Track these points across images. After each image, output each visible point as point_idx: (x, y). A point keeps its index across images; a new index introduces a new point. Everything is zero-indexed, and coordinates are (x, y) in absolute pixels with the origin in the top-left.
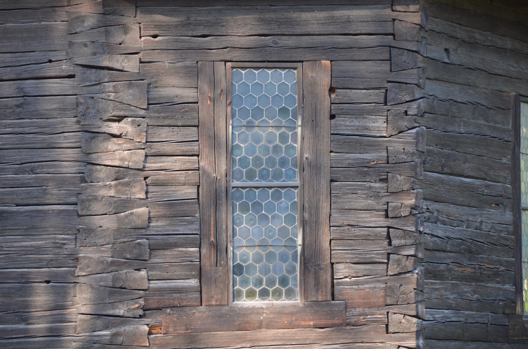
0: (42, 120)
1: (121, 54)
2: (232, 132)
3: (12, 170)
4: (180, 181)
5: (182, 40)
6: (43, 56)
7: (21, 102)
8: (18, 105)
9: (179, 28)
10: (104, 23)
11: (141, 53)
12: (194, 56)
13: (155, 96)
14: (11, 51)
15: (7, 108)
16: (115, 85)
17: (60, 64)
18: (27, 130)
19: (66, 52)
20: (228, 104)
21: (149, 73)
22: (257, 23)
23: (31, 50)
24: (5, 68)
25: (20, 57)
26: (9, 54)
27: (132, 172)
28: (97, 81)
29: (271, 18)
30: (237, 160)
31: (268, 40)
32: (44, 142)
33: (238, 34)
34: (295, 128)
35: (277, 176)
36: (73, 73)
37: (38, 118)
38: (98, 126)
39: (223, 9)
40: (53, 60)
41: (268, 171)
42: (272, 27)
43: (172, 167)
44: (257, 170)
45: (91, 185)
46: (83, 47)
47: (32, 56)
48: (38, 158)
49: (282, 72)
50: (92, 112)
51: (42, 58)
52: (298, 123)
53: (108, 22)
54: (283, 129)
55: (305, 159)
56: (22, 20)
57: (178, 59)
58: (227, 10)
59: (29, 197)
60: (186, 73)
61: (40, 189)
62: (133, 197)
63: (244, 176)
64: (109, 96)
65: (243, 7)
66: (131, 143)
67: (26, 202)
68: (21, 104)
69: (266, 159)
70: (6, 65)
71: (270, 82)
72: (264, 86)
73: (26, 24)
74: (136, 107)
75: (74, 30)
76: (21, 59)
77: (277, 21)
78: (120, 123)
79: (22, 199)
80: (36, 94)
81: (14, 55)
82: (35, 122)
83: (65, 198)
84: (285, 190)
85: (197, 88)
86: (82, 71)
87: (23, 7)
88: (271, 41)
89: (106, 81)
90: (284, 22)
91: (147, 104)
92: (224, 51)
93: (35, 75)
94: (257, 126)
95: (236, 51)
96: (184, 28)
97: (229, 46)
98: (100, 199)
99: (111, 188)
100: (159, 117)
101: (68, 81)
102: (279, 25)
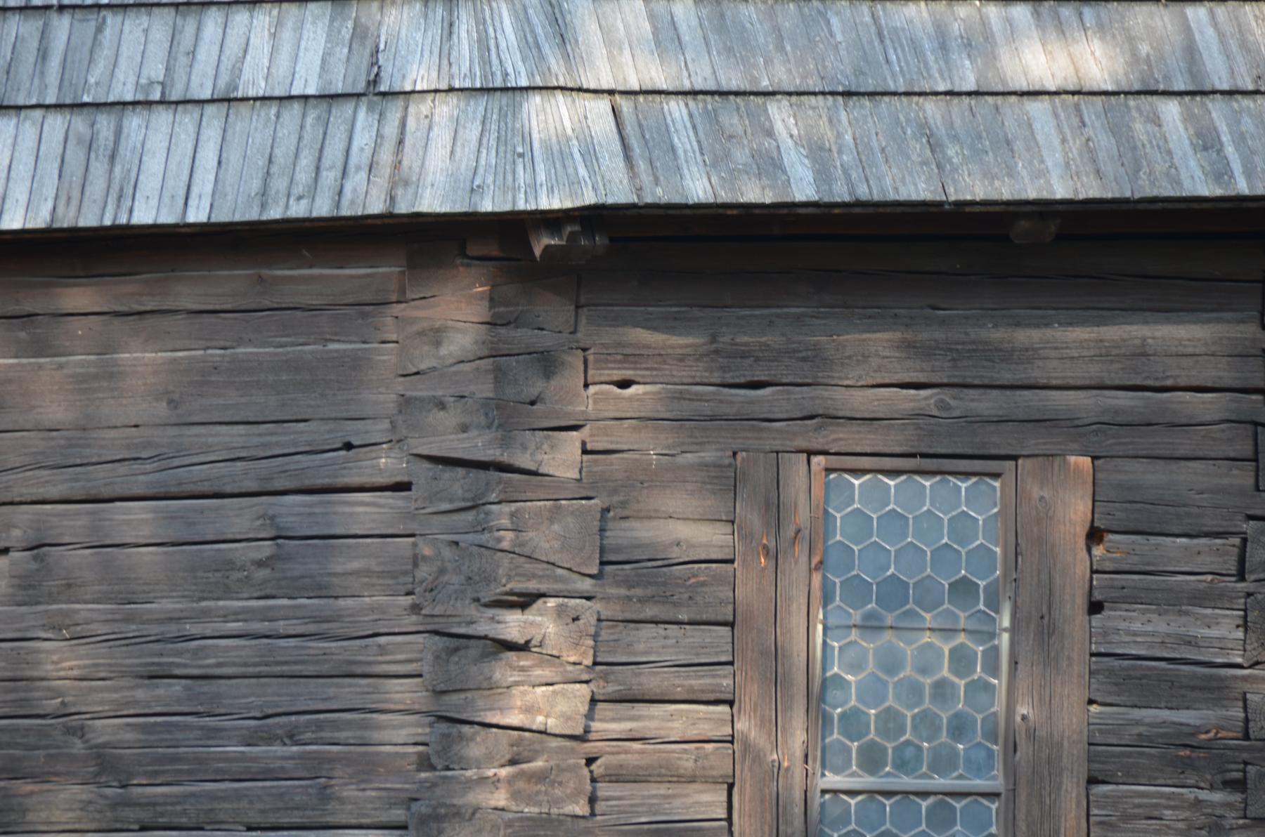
0: (322, 601)
2: (825, 643)
3: (237, 733)
4: (682, 771)
5: (696, 394)
6: (330, 432)
8: (261, 560)
9: (691, 363)
10: (492, 349)
13: (620, 541)
15: (232, 569)
16: (517, 510)
17: (374, 455)
18: (281, 626)
19: (391, 422)
20: (813, 566)
21: (607, 481)
24: (229, 464)
25: (271, 434)
26: (241, 427)
27: (554, 743)
28: (468, 500)
29: (935, 340)
30: (836, 716)
31: (926, 398)
32: (326, 660)
34: (992, 635)
35: (943, 763)
36: (405, 479)
37: (312, 595)
38: (469, 619)
40: (355, 443)
41: (919, 748)
42: (937, 363)
43: (662, 733)
44: (890, 746)
45: (445, 777)
46: (435, 410)
47: (302, 432)
48: (310, 702)
49: (959, 483)
50: (452, 582)
51: (327, 436)
52: (1001, 620)
53: (501, 346)
54: (962, 638)
55: (1018, 719)
56: (278, 339)
57: (683, 444)
58: (817, 318)
59: (280, 805)
60: (704, 483)
61: (311, 786)
62: (555, 811)
63: (854, 762)
64: (499, 540)
65: (861, 311)
66: (553, 665)
67: (273, 820)
68: (268, 558)
69: (914, 718)
71: (929, 510)
72: (911, 521)
74: (570, 569)
75: (413, 365)
76: (274, 439)
77: (950, 350)
78: (527, 612)
79: (262, 811)
80: (309, 533)
81: (255, 429)
82: (304, 606)
83: (375, 809)
84: (965, 802)
85: (733, 522)
87: (284, 306)
88: (932, 401)
90: (969, 351)
91: (598, 561)
92: (806, 425)
93: (307, 483)
94: (891, 627)
95: (838, 425)
96: (700, 364)
97: (821, 412)
98: (467, 816)
99: (499, 785)
100: (629, 598)
102: (954, 360)
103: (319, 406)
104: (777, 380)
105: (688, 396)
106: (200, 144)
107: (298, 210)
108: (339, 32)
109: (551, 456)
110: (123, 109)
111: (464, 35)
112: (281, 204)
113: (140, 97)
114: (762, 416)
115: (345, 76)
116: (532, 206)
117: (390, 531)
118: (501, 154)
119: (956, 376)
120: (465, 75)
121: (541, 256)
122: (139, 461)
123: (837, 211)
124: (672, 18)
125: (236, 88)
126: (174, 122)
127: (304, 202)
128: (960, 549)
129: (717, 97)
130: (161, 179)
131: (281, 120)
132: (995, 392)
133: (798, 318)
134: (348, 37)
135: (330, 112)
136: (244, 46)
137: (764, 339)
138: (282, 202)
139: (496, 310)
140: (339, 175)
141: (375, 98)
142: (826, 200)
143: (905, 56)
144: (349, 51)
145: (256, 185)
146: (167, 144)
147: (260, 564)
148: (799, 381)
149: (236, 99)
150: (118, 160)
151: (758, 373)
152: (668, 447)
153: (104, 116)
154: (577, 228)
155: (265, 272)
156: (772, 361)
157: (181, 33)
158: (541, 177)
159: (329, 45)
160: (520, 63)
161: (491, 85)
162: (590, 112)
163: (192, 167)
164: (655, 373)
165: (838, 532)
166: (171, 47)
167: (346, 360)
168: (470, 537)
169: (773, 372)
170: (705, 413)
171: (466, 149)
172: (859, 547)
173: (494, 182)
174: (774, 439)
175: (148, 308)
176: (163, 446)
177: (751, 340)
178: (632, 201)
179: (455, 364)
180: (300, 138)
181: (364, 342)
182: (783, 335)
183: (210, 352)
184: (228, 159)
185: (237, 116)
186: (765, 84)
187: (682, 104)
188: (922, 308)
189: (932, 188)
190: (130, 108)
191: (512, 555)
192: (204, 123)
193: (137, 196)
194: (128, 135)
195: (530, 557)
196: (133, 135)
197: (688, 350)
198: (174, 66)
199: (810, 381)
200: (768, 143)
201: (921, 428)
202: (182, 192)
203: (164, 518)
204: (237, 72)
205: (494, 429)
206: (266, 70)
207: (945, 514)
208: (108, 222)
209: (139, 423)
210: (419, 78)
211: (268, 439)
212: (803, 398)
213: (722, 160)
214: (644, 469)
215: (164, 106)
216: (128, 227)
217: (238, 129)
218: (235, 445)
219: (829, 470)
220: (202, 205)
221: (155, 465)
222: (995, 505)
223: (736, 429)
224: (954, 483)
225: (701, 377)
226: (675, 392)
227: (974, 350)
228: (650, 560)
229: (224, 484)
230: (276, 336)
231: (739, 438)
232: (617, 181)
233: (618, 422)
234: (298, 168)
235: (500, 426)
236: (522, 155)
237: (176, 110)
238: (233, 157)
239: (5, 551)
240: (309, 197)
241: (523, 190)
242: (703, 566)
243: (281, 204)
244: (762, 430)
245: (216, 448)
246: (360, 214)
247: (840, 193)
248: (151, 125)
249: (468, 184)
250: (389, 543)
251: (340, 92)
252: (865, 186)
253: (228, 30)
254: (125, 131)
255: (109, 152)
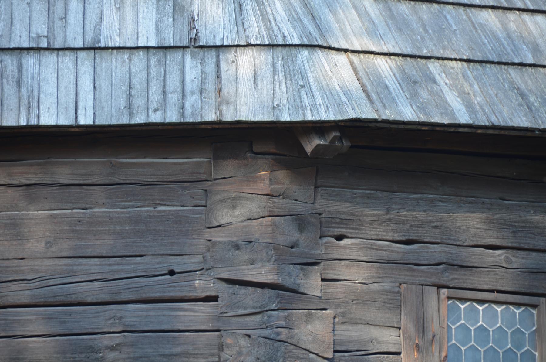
1: (295, 264)
5: (379, 246)
6: (159, 263)
7: (117, 342)
8: (113, 346)
9: (376, 226)
10: (270, 211)
11: (322, 264)
12: (396, 274)
13: (342, 338)
14: (100, 255)
15: (92, 352)
16: (288, 315)
17: (190, 278)
19: (203, 258)
21: (335, 299)
22: (484, 227)
23: (138, 254)
24: (89, 283)
25: (118, 264)
26: (96, 260)
28: (257, 308)
29: (504, 219)
31: (499, 255)
33: (458, 243)
36: (213, 294)
39: (435, 199)
40: (177, 270)
42: (505, 234)
46: (233, 250)
47: (140, 263)
49: (515, 310)
51: (158, 266)
53: (275, 210)
56: (123, 203)
57: (373, 277)
58: (442, 201)
60: (385, 303)
64: (278, 334)
65: (464, 198)
68: (117, 345)
70: (91, 279)
71: (500, 326)
72: (491, 333)
73: (131, 210)
74: (317, 354)
75: (217, 221)
76: (120, 267)
77: (512, 226)
81: (106, 261)
85: (400, 328)
86: (231, 291)
87: (128, 182)
88: (502, 257)
89: (272, 308)
90: (522, 227)
91: (333, 350)
92: (437, 269)
93: (145, 296)
95: (454, 270)
96: (381, 227)
97: (445, 261)
101: (203, 306)
102: (514, 232)
103: (151, 247)
104: (422, 239)
105: (375, 247)
106: (79, 76)
107: (156, 118)
108: (165, 8)
109: (305, 281)
110: (20, 53)
111: (250, 12)
112: (143, 114)
113: (33, 45)
114: (414, 262)
115: (173, 35)
116: (316, 118)
117: (203, 328)
118: (289, 86)
119: (516, 243)
120: (257, 36)
121: (312, 152)
122: (26, 282)
123: (479, 131)
124: (365, 9)
125: (99, 41)
126: (58, 61)
127: (159, 113)
128: (517, 352)
129: (401, 58)
130: (56, 97)
131: (133, 62)
132: (534, 254)
133: (432, 202)
134: (171, 11)
135: (166, 57)
136: (99, 15)
137: (414, 213)
138: (144, 113)
139: (273, 186)
140: (180, 97)
141: (196, 50)
142: (476, 123)
143: (491, 40)
144: (174, 20)
145: (123, 102)
146: (56, 75)
147: (112, 348)
148: (434, 241)
149: (100, 48)
150: (23, 85)
151: (412, 234)
152: (365, 279)
153: (8, 57)
154: (338, 134)
155: (114, 160)
156: (419, 227)
157: (54, 6)
158: (319, 100)
159: (159, 16)
160: (292, 30)
161: (275, 43)
162: (337, 62)
163: (76, 90)
164: (357, 231)
165: (453, 338)
166: (48, 14)
167: (171, 217)
168: (258, 332)
169: (419, 234)
170: (384, 258)
171: (265, 82)
172: (465, 348)
173: (288, 102)
174: (421, 277)
175: (33, 182)
176: (42, 272)
177: (408, 213)
178: (374, 117)
179: (245, 220)
180: (148, 74)
181: (182, 206)
182: (424, 211)
183: (75, 211)
184: (100, 85)
185: (101, 59)
186: (425, 52)
187: (384, 61)
188: (496, 198)
189: (530, 120)
190: (26, 52)
191: (286, 344)
192: (79, 63)
193: (41, 107)
194: (27, 69)
195: (296, 346)
196: (31, 69)
197: (374, 218)
198: (53, 26)
199: (439, 241)
200: (435, 87)
201: (497, 274)
202: (73, 105)
203: (43, 319)
204: (98, 31)
205: (272, 263)
206: (118, 31)
207: (509, 329)
208: (23, 123)
209: (25, 257)
210: (225, 37)
211: (116, 267)
212: (435, 252)
213: (415, 96)
214: (354, 292)
215: (49, 51)
216: (38, 127)
217: (103, 67)
218: (93, 271)
219: (449, 298)
220: (88, 114)
221: (37, 284)
222: (534, 326)
223: (400, 269)
224: (513, 310)
225: (382, 235)
226: (368, 244)
227: (525, 227)
228: (358, 351)
229: (86, 297)
230: (122, 201)
231: (402, 275)
232: (364, 104)
233: (339, 262)
234: (150, 92)
235: (275, 260)
236: (302, 87)
237: (58, 54)
238: (103, 84)
239: (545, 261)
240: (162, 110)
241: (308, 108)
242: (386, 356)
243: (143, 114)
244: (414, 270)
245: (79, 273)
246: (199, 121)
247: (482, 120)
248: (42, 63)
249: (270, 104)
250: (201, 335)
251: (172, 45)
252: (494, 117)
253: (86, 5)
254: (25, 66)
255: (15, 80)
